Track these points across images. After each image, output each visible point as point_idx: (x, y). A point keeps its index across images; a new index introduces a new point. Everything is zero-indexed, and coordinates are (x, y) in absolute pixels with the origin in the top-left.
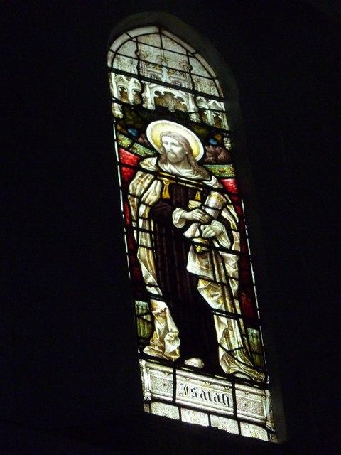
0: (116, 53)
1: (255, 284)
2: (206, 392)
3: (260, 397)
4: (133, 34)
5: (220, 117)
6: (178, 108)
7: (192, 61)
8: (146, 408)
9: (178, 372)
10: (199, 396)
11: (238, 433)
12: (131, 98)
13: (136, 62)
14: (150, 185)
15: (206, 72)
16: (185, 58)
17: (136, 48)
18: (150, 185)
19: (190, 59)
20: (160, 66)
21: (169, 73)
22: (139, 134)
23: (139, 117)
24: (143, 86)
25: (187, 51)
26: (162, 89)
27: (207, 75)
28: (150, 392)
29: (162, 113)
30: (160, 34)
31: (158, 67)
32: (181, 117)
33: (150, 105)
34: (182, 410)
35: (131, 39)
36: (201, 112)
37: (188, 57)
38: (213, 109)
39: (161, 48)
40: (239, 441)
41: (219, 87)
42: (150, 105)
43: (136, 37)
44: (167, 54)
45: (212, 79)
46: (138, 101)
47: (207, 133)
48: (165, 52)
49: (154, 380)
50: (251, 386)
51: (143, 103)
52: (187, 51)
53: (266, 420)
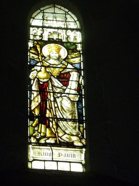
4: (42, 9)
8: (29, 166)
9: (52, 148)
10: (63, 155)
12: (38, 38)
15: (73, 20)
17: (43, 15)
20: (52, 20)
24: (43, 30)
25: (66, 12)
26: (52, 30)
27: (73, 21)
32: (59, 42)
37: (66, 14)
38: (77, 37)
41: (49, 7)
43: (43, 10)
44: (56, 15)
45: (75, 22)
47: (71, 48)
50: (46, 146)
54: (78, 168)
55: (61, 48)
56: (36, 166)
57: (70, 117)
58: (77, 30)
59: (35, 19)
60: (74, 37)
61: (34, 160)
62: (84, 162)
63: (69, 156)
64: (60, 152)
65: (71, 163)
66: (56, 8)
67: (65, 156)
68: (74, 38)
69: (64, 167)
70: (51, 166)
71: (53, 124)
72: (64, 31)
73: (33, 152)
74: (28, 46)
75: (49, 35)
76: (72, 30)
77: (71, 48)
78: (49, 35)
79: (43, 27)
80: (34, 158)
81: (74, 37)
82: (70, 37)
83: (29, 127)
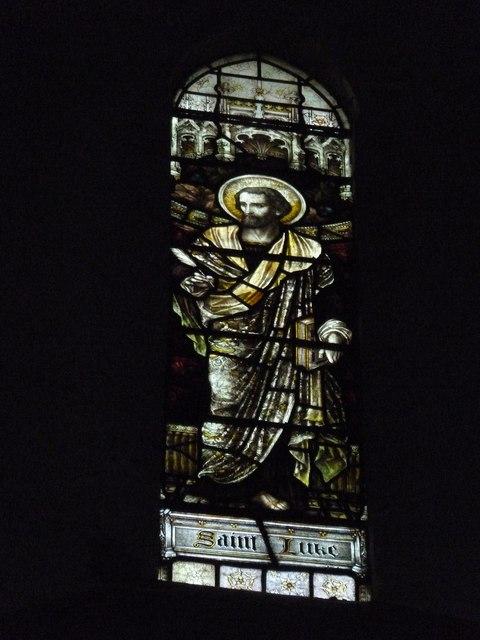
2: (243, 537)
3: (349, 537)
5: (338, 159)
11: (213, 584)
13: (215, 100)
29: (247, 163)
31: (249, 104)
32: (276, 166)
36: (308, 156)
44: (266, 85)
47: (306, 178)
48: (265, 83)
54: (344, 589)
56: (186, 574)
67: (223, 542)
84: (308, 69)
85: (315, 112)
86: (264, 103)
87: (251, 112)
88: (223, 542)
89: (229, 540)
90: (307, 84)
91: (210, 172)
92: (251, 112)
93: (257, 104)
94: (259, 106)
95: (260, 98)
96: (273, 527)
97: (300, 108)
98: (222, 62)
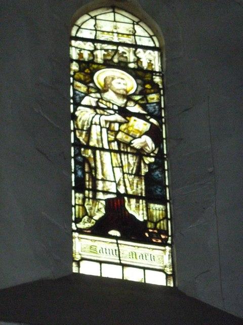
0: (80, 28)
1: (166, 139)
4: (93, 14)
6: (120, 60)
7: (137, 27)
14: (121, 158)
16: (132, 26)
18: (121, 158)
19: (135, 26)
21: (118, 36)
22: (88, 80)
23: (89, 67)
25: (134, 21)
27: (147, 35)
28: (80, 254)
29: (108, 64)
30: (114, 12)
31: (111, 34)
32: (123, 66)
33: (100, 60)
34: (146, 271)
35: (92, 18)
36: (138, 60)
37: (134, 24)
38: (151, 59)
39: (115, 21)
40: (142, 287)
42: (100, 60)
43: (96, 16)
44: (118, 24)
45: (151, 37)
46: (91, 58)
47: (140, 74)
48: (118, 23)
49: (82, 245)
51: (94, 59)
52: (134, 21)
53: (165, 267)
54: (158, 280)
55: (146, 141)
56: (88, 269)
57: (116, 148)
58: (153, 49)
59: (89, 51)
60: (149, 61)
61: (83, 259)
62: (169, 271)
63: (153, 259)
64: (130, 250)
65: (146, 271)
66: (116, 14)
67: (101, 251)
68: (148, 63)
69: (133, 275)
70: (112, 272)
71: (117, 203)
72: (132, 49)
73: (167, 261)
74: (70, 70)
75: (104, 55)
76: (146, 48)
77: (140, 74)
78: (104, 55)
79: (94, 41)
80: (83, 256)
81: (149, 61)
82: (141, 60)
83: (75, 207)
84: (141, 18)
85: (142, 38)
86: (118, 33)
87: (112, 38)
88: (101, 251)
89: (104, 250)
90: (137, 24)
91: (89, 67)
92: (112, 38)
93: (114, 34)
94: (116, 35)
95: (115, 31)
96: (75, 215)
97: (134, 35)
98: (99, 11)
